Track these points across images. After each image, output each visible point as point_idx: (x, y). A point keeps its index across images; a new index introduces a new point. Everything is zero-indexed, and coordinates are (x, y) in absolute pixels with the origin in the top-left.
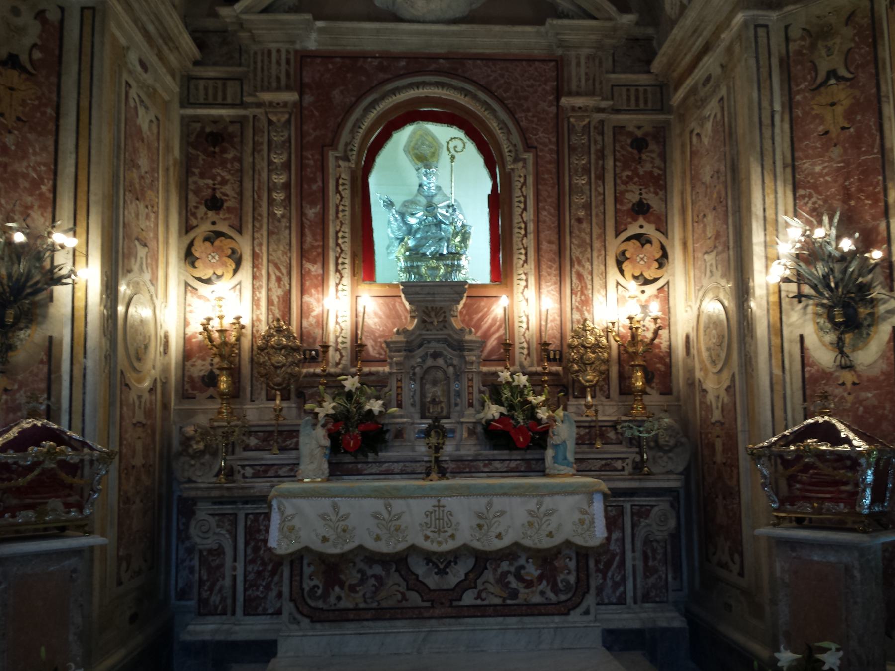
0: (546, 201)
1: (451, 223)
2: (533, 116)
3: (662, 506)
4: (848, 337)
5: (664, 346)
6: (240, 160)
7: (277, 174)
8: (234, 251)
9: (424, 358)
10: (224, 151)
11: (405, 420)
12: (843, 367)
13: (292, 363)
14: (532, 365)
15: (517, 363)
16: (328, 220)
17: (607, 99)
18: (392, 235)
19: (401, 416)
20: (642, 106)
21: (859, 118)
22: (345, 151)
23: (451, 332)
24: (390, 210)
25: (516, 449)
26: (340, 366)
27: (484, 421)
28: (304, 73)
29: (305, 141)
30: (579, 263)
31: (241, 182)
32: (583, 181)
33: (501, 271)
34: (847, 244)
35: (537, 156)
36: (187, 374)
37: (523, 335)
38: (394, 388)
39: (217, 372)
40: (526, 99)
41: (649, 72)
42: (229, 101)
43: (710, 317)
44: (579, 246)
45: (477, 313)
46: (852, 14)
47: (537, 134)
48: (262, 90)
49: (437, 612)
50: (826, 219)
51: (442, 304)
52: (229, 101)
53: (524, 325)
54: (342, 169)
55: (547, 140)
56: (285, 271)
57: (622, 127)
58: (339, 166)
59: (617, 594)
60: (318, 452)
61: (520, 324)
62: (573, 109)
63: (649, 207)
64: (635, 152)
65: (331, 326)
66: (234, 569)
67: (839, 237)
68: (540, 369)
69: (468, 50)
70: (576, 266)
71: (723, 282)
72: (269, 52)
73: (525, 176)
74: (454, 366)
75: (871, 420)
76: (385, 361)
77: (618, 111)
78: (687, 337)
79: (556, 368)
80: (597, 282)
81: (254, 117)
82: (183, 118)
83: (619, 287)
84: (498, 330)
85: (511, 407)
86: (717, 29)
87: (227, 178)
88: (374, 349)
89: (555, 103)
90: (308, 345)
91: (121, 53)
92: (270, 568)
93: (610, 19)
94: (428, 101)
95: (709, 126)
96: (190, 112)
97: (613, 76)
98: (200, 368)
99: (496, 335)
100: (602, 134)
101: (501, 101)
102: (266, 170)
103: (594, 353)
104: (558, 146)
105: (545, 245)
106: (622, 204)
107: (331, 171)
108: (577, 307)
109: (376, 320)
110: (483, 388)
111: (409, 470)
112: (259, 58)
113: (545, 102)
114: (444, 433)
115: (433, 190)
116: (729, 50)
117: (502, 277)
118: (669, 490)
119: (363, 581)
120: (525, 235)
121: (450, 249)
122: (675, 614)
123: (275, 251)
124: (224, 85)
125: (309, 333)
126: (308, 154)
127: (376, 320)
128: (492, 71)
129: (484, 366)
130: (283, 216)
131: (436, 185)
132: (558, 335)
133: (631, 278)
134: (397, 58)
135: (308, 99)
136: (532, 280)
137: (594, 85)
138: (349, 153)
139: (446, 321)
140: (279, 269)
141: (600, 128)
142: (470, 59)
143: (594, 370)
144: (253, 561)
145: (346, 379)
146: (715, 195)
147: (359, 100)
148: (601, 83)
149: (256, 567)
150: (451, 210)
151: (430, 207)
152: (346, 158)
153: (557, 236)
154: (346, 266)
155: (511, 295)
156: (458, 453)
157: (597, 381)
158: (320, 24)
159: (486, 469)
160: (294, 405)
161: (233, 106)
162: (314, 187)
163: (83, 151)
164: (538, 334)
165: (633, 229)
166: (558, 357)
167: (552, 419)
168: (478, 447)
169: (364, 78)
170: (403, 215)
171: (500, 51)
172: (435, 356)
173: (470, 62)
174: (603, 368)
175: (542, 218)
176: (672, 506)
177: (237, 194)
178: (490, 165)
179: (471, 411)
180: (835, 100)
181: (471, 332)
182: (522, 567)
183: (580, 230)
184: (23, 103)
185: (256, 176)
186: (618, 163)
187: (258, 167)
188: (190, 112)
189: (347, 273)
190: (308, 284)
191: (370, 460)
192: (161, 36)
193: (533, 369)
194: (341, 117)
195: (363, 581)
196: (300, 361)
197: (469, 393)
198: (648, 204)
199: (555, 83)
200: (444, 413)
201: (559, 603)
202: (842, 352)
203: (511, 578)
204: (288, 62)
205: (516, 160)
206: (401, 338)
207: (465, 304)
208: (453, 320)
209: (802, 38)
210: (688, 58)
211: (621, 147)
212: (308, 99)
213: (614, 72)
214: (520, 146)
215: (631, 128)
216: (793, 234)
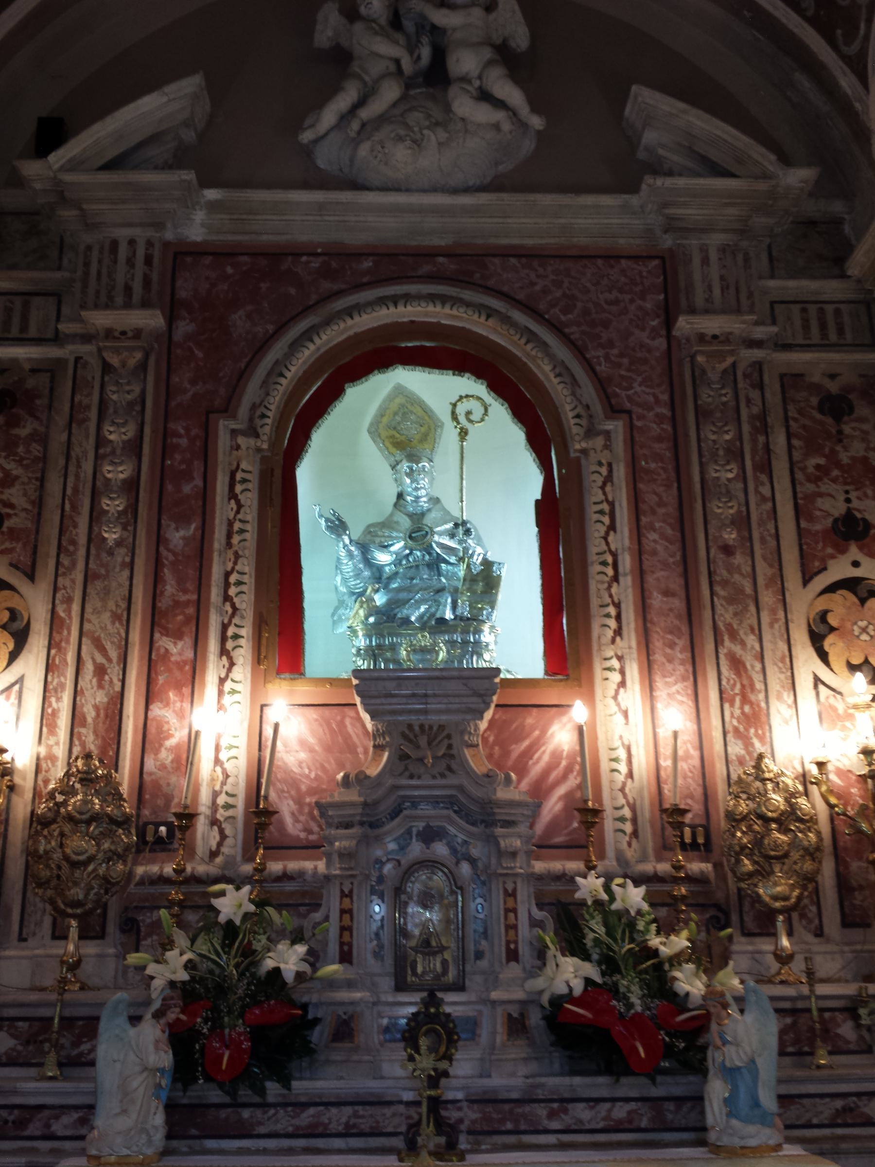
0: (654, 512)
1: (461, 560)
2: (621, 355)
6: (43, 439)
7: (112, 463)
8: (14, 614)
11: (358, 995)
13: (112, 856)
14: (643, 859)
15: (610, 852)
16: (211, 551)
18: (343, 589)
19: (350, 985)
20: (833, 337)
22: (251, 420)
23: (465, 782)
24: (339, 536)
25: (628, 1072)
26: (219, 860)
27: (545, 1000)
28: (179, 283)
29: (173, 404)
30: (734, 635)
31: (42, 480)
33: (567, 652)
35: (631, 428)
37: (622, 790)
38: (335, 915)
40: (606, 324)
41: (843, 276)
42: (33, 332)
44: (730, 601)
45: (518, 740)
47: (630, 388)
52: (33, 332)
53: (623, 768)
54: (242, 453)
55: (651, 399)
56: (114, 654)
57: (800, 376)
58: (238, 447)
60: (139, 1084)
61: (615, 765)
62: (701, 338)
64: (829, 420)
65: (205, 766)
68: (664, 868)
69: (492, 241)
70: (727, 642)
73: (610, 465)
74: (473, 861)
76: (316, 846)
77: (787, 347)
79: (697, 867)
80: (776, 678)
81: (77, 359)
83: (821, 687)
84: (565, 777)
85: (610, 964)
87: (14, 472)
88: (296, 820)
89: (663, 332)
90: (154, 812)
93: (766, 176)
94: (413, 329)
97: (772, 283)
99: (562, 790)
100: (760, 386)
101: (557, 329)
102: (91, 455)
103: (786, 831)
104: (673, 409)
105: (657, 600)
106: (811, 519)
107: (220, 456)
108: (736, 730)
109: (303, 755)
110: (538, 914)
111: (365, 1125)
112: (95, 254)
113: (643, 329)
114: (450, 1033)
117: (570, 664)
120: (616, 578)
121: (459, 611)
123: (96, 612)
124: (26, 306)
125: (156, 785)
127: (303, 755)
128: (538, 276)
129: (538, 859)
130: (119, 543)
131: (431, 488)
132: (698, 792)
133: (845, 669)
134: (357, 255)
136: (633, 671)
137: (738, 300)
138: (259, 422)
139: (452, 756)
140: (102, 650)
141: (756, 375)
142: (494, 256)
143: (788, 874)
145: (222, 894)
147: (281, 328)
148: (750, 295)
151: (418, 534)
152: (253, 432)
153: (682, 581)
154: (242, 642)
155: (590, 699)
156: (486, 1082)
157: (799, 898)
158: (212, 194)
159: (555, 1125)
160: (112, 951)
161: (38, 341)
162: (187, 489)
164: (654, 789)
165: (840, 569)
166: (701, 840)
167: (715, 997)
168: (533, 1067)
169: (292, 291)
170: (364, 548)
171: (552, 241)
172: (429, 835)
173: (496, 260)
174: (808, 866)
175: (648, 545)
177: (33, 503)
178: (538, 443)
179: (514, 970)
181: (508, 779)
183: (730, 569)
185: (72, 469)
186: (796, 442)
187: (76, 451)
189: (243, 654)
190: (161, 679)
191: (271, 1099)
193: (648, 867)
194: (245, 360)
196: (127, 848)
197: (508, 927)
198: (865, 520)
199: (662, 297)
204: (148, 260)
205: (590, 432)
206: (353, 796)
207: (491, 722)
208: (467, 753)
211: (800, 412)
212: (184, 328)
213: (772, 277)
214: (598, 408)
215: (816, 378)
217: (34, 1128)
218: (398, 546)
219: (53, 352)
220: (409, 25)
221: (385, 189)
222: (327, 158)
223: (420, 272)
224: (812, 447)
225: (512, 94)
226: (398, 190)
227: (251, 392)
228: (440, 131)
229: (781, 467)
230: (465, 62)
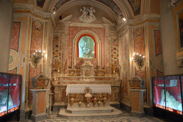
3: (117, 88)
4: (140, 67)
20: (115, 35)
34: (140, 55)
35: (101, 41)
67: (139, 54)
82: (53, 35)
95: (124, 39)
96: (54, 34)
119: (79, 97)
162: (71, 44)
188: (54, 34)
195: (79, 97)
203: (98, 97)
214: (99, 40)
216: (134, 54)
218: (85, 48)
220: (87, 10)
224: (113, 43)
225: (94, 17)
229: (111, 44)
230: (91, 14)
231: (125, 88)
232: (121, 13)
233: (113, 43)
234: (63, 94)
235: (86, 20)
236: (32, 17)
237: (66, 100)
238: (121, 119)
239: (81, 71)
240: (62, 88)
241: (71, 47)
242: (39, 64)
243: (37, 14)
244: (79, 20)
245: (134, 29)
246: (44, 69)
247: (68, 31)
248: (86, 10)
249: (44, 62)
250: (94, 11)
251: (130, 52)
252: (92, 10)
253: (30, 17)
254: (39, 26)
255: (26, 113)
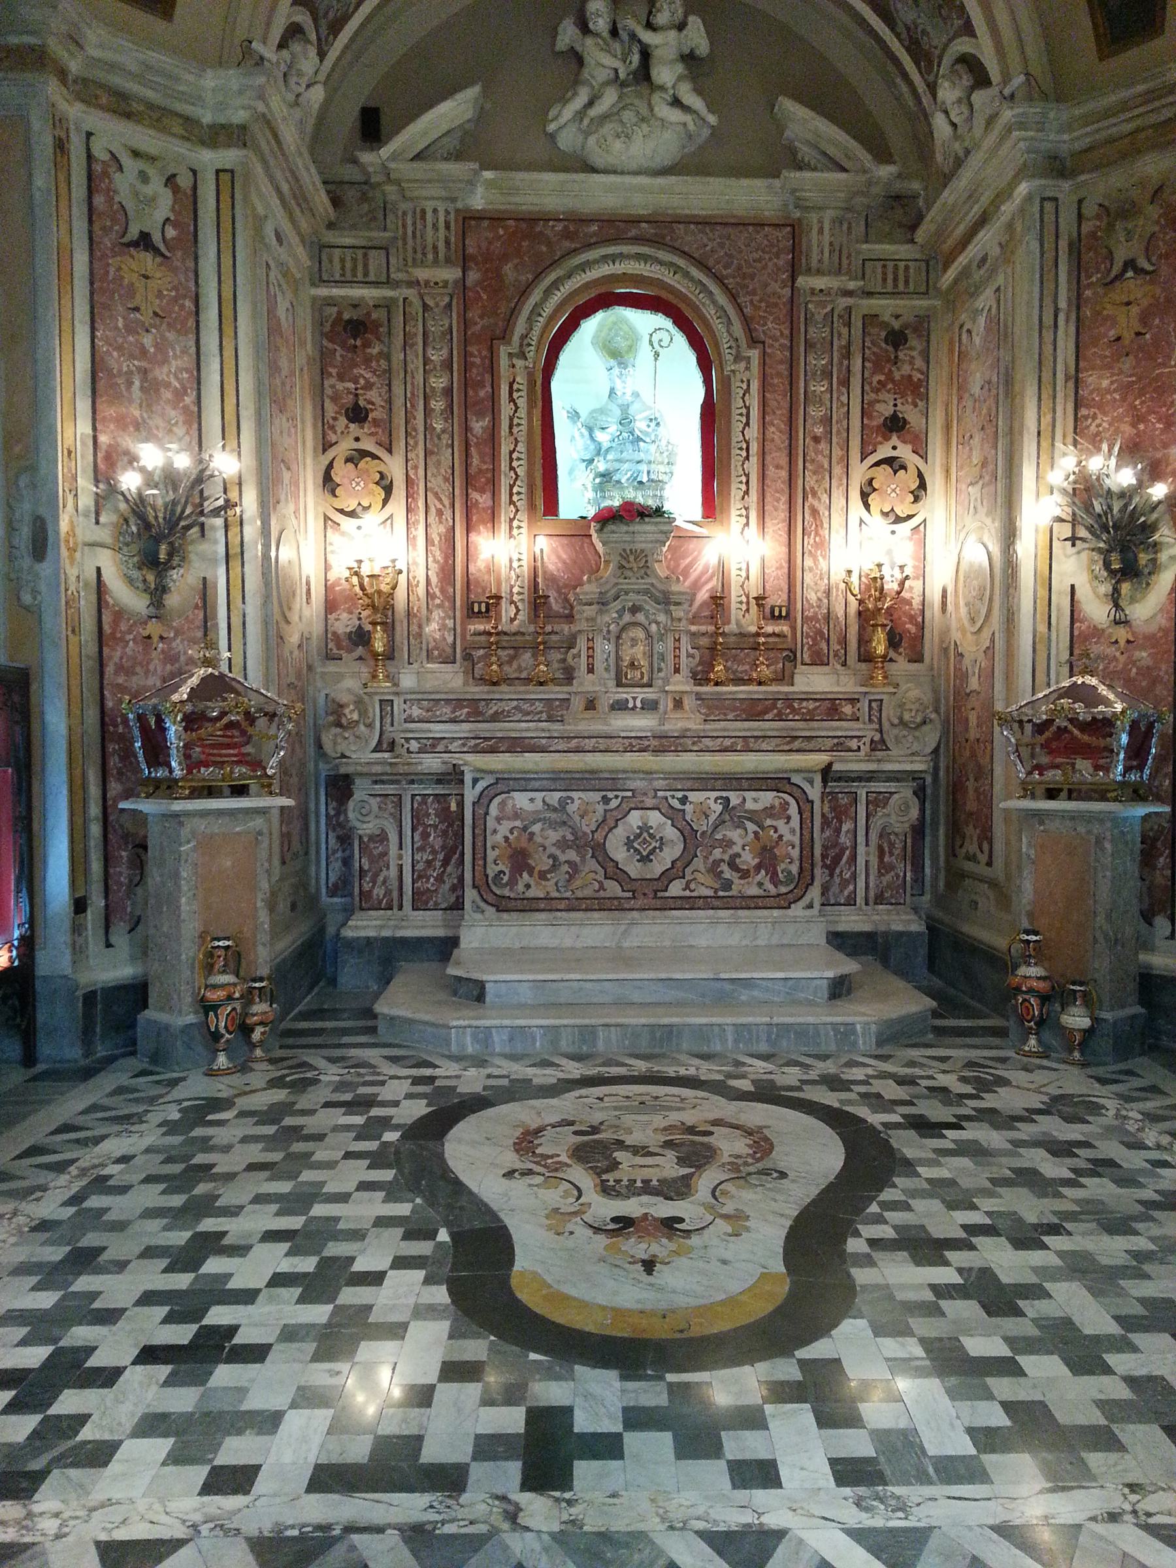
2: (760, 301)
3: (904, 793)
4: (1125, 587)
5: (916, 603)
9: (621, 613)
10: (367, 344)
12: (1117, 622)
15: (733, 618)
17: (856, 279)
20: (901, 287)
21: (1157, 321)
22: (521, 345)
31: (389, 385)
32: (820, 388)
33: (711, 506)
36: (330, 629)
39: (369, 627)
41: (912, 241)
43: (971, 565)
45: (684, 558)
46: (1159, 189)
48: (415, 265)
49: (639, 903)
50: (1105, 447)
51: (643, 546)
52: (372, 278)
56: (447, 502)
59: (846, 893)
62: (813, 291)
63: (905, 421)
64: (890, 348)
66: (400, 857)
71: (988, 521)
72: (423, 212)
74: (658, 623)
75: (1144, 684)
77: (870, 294)
78: (944, 591)
86: (997, 196)
91: (258, 223)
92: (441, 856)
95: (982, 320)
96: (323, 292)
97: (864, 246)
98: (344, 623)
99: (709, 586)
100: (849, 325)
101: (719, 280)
102: (421, 370)
105: (771, 471)
106: (870, 417)
115: (628, 398)
116: (1010, 226)
118: (913, 776)
119: (555, 867)
120: (747, 458)
122: (913, 917)
124: (365, 255)
125: (477, 582)
126: (473, 349)
130: (443, 431)
134: (585, 221)
135: (473, 276)
140: (440, 500)
144: (422, 849)
146: (984, 411)
147: (538, 277)
149: (427, 856)
150: (653, 424)
151: (625, 421)
158: (488, 175)
161: (376, 284)
162: (482, 394)
163: (229, 353)
165: (885, 451)
170: (590, 430)
172: (635, 610)
173: (681, 226)
175: (769, 436)
176: (915, 793)
178: (704, 364)
180: (1132, 298)
182: (738, 855)
184: (160, 295)
186: (867, 364)
187: (411, 367)
188: (323, 292)
192: (295, 197)
195: (555, 867)
200: (645, 680)
201: (779, 895)
202: (1117, 605)
203: (724, 867)
204: (448, 227)
205: (738, 358)
208: (656, 565)
209: (1098, 217)
210: (962, 229)
212: (473, 276)
214: (743, 343)
215: (886, 318)
217: (440, 748)
219: (388, 293)
220: (624, 35)
221: (606, 172)
222: (568, 140)
223: (630, 235)
224: (878, 368)
225: (696, 102)
226: (615, 172)
227: (520, 327)
228: (644, 126)
229: (856, 382)
230: (665, 74)
231: (971, 784)
232: (962, 46)
233: (878, 368)
234: (425, 836)
235: (618, 145)
236: (74, 111)
237: (453, 889)
238: (912, 1064)
239: (582, 644)
240: (417, 789)
241: (486, 421)
242: (182, 583)
243: (116, 80)
244: (552, 137)
245: (1090, 209)
246: (236, 621)
247: (448, 261)
248: (614, 32)
249: (235, 564)
250: (697, 37)
251: (1029, 447)
252: (673, 34)
253: (58, 121)
254: (157, 212)
255: (90, 998)
